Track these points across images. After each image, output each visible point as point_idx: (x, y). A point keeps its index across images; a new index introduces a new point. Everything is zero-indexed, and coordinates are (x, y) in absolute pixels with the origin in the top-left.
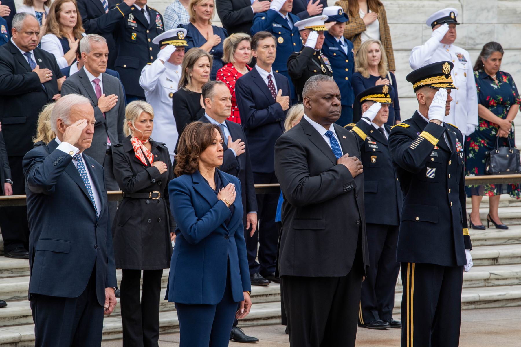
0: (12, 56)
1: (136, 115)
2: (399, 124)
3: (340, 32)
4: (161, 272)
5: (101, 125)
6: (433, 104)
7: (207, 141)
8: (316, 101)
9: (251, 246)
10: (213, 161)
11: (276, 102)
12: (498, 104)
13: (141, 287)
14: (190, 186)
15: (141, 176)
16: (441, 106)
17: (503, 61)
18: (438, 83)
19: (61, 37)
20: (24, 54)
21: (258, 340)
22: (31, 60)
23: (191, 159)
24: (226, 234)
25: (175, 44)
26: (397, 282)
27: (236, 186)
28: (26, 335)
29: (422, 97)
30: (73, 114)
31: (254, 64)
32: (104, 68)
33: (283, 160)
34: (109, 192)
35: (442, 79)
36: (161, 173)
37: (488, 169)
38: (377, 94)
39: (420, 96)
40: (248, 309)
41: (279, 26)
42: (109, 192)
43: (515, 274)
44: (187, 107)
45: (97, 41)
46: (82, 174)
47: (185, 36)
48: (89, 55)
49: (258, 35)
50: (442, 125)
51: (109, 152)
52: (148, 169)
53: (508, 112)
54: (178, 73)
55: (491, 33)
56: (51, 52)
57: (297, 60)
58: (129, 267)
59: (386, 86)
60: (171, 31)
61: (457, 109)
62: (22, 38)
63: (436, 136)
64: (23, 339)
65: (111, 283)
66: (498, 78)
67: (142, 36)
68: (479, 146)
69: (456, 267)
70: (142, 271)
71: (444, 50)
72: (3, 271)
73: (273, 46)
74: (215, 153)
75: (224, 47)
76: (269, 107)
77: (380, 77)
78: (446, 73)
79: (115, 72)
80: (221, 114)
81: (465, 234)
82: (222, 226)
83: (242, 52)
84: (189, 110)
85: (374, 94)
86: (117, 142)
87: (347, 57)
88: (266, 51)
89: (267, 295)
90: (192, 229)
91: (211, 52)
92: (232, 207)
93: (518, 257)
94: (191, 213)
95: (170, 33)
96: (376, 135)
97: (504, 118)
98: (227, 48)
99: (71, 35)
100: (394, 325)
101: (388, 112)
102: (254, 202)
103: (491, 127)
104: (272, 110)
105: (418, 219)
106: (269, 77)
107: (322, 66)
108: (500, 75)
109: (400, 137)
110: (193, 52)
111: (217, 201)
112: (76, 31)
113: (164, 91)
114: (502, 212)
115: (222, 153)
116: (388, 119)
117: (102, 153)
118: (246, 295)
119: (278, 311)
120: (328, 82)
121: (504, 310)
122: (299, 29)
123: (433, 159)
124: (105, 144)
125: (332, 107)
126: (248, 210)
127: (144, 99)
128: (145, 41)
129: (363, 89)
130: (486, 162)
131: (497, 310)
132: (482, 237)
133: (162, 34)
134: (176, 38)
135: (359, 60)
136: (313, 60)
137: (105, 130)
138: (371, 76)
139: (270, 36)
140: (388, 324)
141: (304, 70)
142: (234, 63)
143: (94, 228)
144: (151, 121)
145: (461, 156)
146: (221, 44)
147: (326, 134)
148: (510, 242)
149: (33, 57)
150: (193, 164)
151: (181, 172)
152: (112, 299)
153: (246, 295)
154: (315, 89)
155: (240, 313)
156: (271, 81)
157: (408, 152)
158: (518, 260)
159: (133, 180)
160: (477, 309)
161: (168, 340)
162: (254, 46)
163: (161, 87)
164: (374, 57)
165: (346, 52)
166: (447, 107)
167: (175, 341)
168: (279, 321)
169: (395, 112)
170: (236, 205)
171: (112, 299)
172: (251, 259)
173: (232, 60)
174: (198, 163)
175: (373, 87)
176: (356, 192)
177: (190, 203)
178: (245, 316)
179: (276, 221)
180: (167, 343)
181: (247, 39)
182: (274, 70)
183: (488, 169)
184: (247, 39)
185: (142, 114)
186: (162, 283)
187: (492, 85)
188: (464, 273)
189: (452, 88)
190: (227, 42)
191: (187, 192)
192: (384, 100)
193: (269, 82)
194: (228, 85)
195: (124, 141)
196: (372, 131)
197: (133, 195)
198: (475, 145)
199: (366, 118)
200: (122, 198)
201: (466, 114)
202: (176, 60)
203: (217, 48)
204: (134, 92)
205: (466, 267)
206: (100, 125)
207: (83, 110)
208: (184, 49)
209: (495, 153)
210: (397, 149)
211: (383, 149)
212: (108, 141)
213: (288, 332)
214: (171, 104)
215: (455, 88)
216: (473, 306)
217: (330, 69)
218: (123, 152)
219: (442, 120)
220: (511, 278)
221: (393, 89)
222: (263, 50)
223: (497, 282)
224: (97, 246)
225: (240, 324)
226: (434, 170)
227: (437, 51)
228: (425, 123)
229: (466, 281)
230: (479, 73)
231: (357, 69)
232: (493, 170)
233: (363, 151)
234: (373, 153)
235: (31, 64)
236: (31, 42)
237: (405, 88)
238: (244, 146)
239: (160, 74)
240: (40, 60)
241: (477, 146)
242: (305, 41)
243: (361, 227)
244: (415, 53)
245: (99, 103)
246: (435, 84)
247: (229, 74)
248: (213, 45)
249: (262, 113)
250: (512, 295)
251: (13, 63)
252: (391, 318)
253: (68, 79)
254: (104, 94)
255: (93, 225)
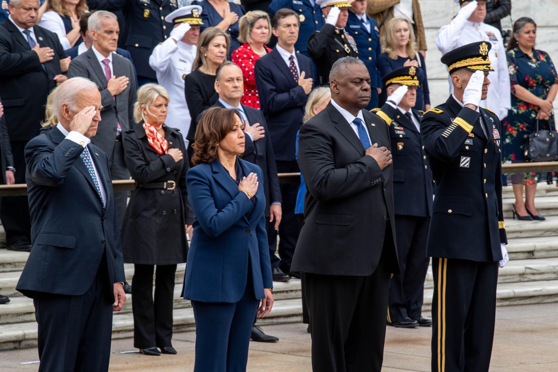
0: (9, 34)
1: (151, 99)
2: (431, 108)
3: (362, 9)
4: (175, 267)
5: (111, 109)
6: (468, 87)
7: (226, 127)
8: (345, 85)
9: (272, 241)
10: (234, 148)
11: (298, 85)
12: (537, 83)
13: (154, 283)
14: (209, 175)
15: (155, 165)
16: (477, 89)
17: (537, 40)
18: (475, 65)
19: (63, 15)
20: (23, 32)
21: (278, 339)
22: (31, 39)
23: (210, 147)
24: (247, 227)
25: (189, 22)
26: (427, 277)
27: (258, 175)
28: (31, 333)
29: (458, 80)
30: (80, 99)
31: (275, 45)
32: (114, 46)
33: (308, 149)
34: (114, 182)
35: (479, 60)
36: (176, 161)
37: (526, 153)
38: (404, 76)
39: (455, 79)
40: (269, 307)
41: (300, 3)
42: (114, 182)
43: (552, 268)
44: (200, 91)
45: (107, 17)
46: (87, 163)
47: (200, 13)
48: (99, 32)
49: (280, 13)
50: (478, 111)
51: (120, 138)
52: (162, 157)
53: (548, 92)
54: (192, 53)
55: (527, 9)
56: (53, 31)
57: (316, 39)
58: (142, 262)
59: (412, 67)
60: (184, 9)
61: (490, 92)
62: (20, 14)
63: (470, 123)
64: (27, 337)
65: (121, 278)
66: (535, 56)
67: (155, 14)
68: (518, 130)
69: (492, 262)
70: (155, 266)
71: (473, 29)
72: (6, 265)
73: (295, 25)
74: (235, 141)
75: (240, 26)
76: (291, 90)
77: (409, 58)
78: (484, 54)
79: (126, 52)
80: (228, 97)
81: (500, 227)
82: (242, 219)
83: (259, 31)
84: (201, 94)
85: (400, 76)
86: (128, 128)
87: (370, 35)
88: (287, 30)
89: (287, 292)
90: (213, 220)
91: (228, 31)
92: (254, 198)
93: (555, 250)
94: (210, 204)
95: (184, 11)
96: (404, 121)
97: (545, 98)
98: (243, 27)
99: (73, 13)
100: (424, 323)
101: (415, 95)
102: (278, 193)
103: (530, 109)
104: (294, 93)
105: (450, 211)
106: (291, 58)
107: (346, 45)
108: (538, 54)
109: (433, 123)
110: (209, 31)
111: (238, 192)
112: (80, 8)
113: (177, 73)
114: (539, 202)
115: (243, 140)
116: (416, 103)
117: (112, 140)
118: (268, 292)
119: (299, 309)
120: (357, 65)
121: (541, 306)
122: (322, 7)
123: (467, 148)
124: (115, 130)
125: (361, 92)
126: (271, 201)
127: (155, 81)
128: (158, 18)
129: (390, 71)
130: (524, 147)
131: (532, 307)
132: (517, 228)
133: (176, 11)
134: (191, 16)
135: (386, 39)
136: (336, 40)
137: (115, 114)
138: (399, 57)
139: (292, 14)
140: (416, 322)
141: (325, 49)
142: (251, 43)
143: (100, 222)
144: (166, 105)
145: (498, 143)
146: (237, 23)
147: (354, 122)
148: (547, 234)
149: (33, 35)
150: (211, 153)
151: (198, 161)
152: (124, 297)
153: (268, 292)
154: (343, 73)
155: (262, 311)
156: (293, 62)
157: (440, 140)
158: (555, 253)
159: (147, 168)
160: (512, 305)
161: (182, 339)
162: (274, 23)
163: (174, 68)
164: (402, 36)
165: (369, 30)
166: (483, 90)
167: (189, 340)
168: (300, 319)
169: (425, 96)
170: (258, 196)
171: (124, 297)
172: (272, 252)
173: (249, 40)
174: (217, 152)
175: (402, 67)
176: (384, 185)
177: (209, 194)
178: (267, 314)
179: (297, 212)
180: (181, 342)
181: (264, 17)
182: (296, 50)
183: (526, 153)
184: (264, 17)
185: (157, 99)
186: (176, 279)
187: (530, 64)
188: (500, 268)
189: (490, 70)
190: (243, 20)
191: (207, 182)
192: (411, 83)
193: (291, 64)
194: (243, 68)
195: (136, 128)
196: (398, 117)
197: (146, 186)
198: (512, 130)
199: (391, 101)
200: (133, 188)
201: (498, 96)
202: (190, 39)
203: (234, 27)
204: (145, 75)
205: (502, 263)
206: (108, 109)
207: (91, 95)
208: (199, 27)
209: (534, 137)
210: (430, 136)
211: (411, 135)
212: (119, 126)
213: (309, 331)
214: (183, 86)
215: (493, 70)
216: (507, 303)
217: (355, 49)
218: (135, 139)
219: (477, 104)
220: (548, 273)
221: (421, 70)
222: (284, 29)
223: (533, 277)
224: (104, 241)
225: (259, 322)
226: (469, 159)
227: (464, 29)
228: (460, 107)
229: (502, 276)
230: (515, 51)
231: (384, 49)
232: (532, 155)
233: (391, 139)
234: (400, 140)
235: (30, 42)
236: (29, 18)
237: (436, 69)
238: (263, 131)
239: (173, 54)
240: (41, 39)
241: (515, 130)
242: (326, 17)
243: (388, 223)
244: (442, 33)
245: (108, 85)
246: (471, 66)
247: (245, 56)
248: (230, 23)
249: (283, 97)
250: (548, 291)
251: (10, 41)
252: (420, 316)
253: (75, 59)
254: (115, 76)
255: (100, 218)
